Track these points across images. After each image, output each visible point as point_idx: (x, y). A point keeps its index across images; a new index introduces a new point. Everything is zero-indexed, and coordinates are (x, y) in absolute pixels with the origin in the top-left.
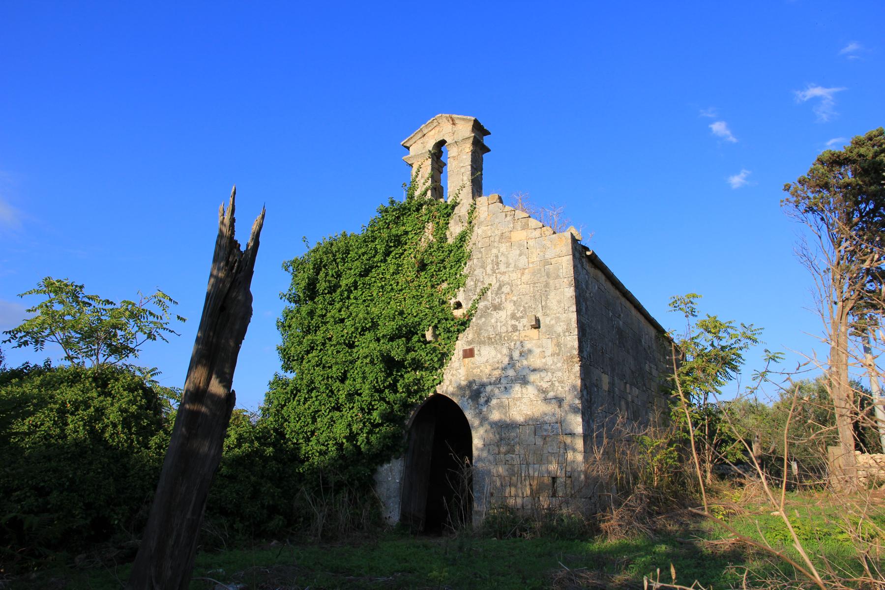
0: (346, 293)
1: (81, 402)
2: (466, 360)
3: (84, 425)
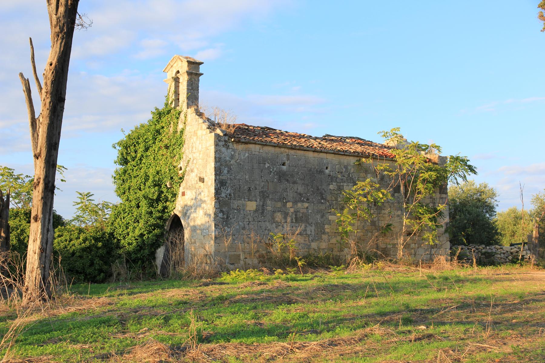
0: (139, 161)
1: (15, 227)
2: (183, 197)
3: (16, 237)
